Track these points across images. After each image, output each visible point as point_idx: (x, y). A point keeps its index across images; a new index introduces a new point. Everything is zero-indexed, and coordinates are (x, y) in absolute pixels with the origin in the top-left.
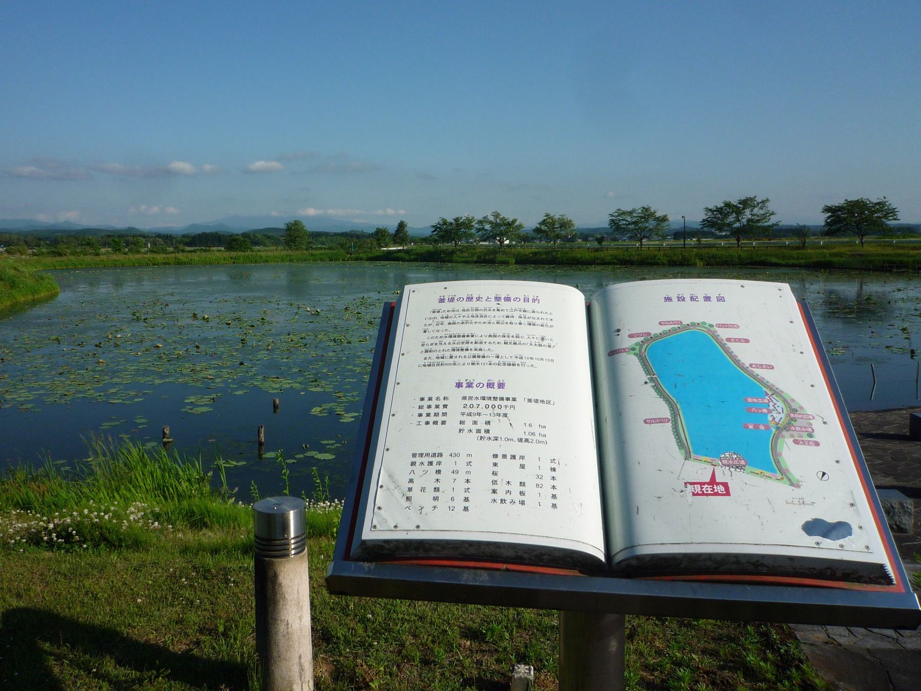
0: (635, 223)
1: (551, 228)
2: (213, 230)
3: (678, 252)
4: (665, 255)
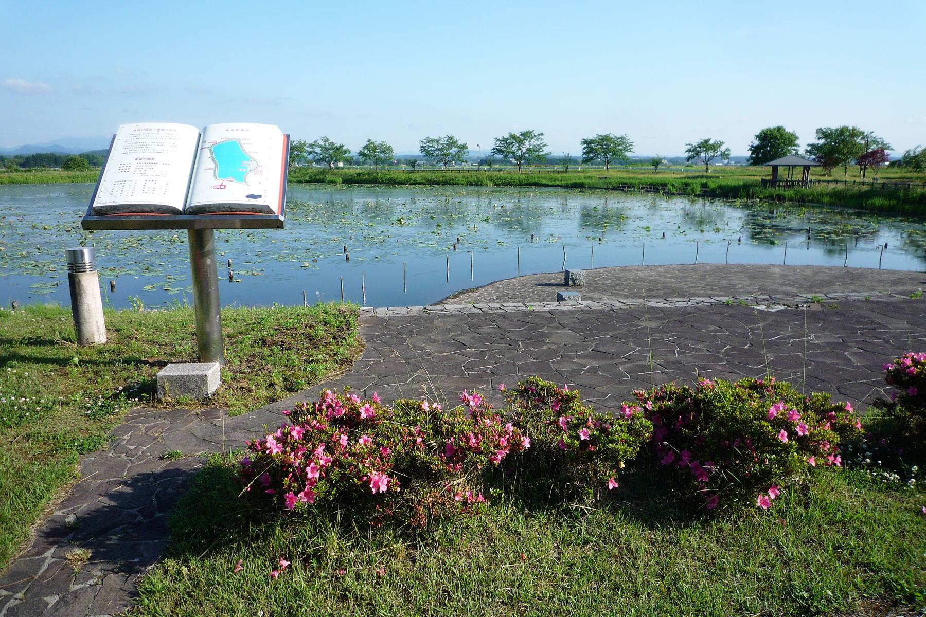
0: (442, 149)
1: (372, 152)
2: (49, 152)
3: (474, 174)
4: (464, 177)
